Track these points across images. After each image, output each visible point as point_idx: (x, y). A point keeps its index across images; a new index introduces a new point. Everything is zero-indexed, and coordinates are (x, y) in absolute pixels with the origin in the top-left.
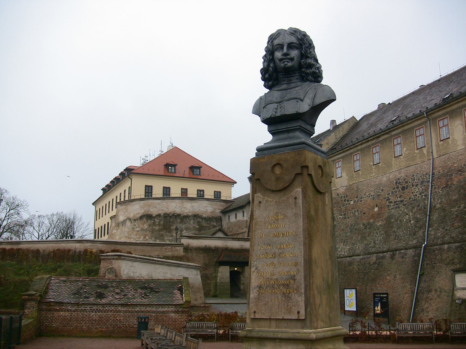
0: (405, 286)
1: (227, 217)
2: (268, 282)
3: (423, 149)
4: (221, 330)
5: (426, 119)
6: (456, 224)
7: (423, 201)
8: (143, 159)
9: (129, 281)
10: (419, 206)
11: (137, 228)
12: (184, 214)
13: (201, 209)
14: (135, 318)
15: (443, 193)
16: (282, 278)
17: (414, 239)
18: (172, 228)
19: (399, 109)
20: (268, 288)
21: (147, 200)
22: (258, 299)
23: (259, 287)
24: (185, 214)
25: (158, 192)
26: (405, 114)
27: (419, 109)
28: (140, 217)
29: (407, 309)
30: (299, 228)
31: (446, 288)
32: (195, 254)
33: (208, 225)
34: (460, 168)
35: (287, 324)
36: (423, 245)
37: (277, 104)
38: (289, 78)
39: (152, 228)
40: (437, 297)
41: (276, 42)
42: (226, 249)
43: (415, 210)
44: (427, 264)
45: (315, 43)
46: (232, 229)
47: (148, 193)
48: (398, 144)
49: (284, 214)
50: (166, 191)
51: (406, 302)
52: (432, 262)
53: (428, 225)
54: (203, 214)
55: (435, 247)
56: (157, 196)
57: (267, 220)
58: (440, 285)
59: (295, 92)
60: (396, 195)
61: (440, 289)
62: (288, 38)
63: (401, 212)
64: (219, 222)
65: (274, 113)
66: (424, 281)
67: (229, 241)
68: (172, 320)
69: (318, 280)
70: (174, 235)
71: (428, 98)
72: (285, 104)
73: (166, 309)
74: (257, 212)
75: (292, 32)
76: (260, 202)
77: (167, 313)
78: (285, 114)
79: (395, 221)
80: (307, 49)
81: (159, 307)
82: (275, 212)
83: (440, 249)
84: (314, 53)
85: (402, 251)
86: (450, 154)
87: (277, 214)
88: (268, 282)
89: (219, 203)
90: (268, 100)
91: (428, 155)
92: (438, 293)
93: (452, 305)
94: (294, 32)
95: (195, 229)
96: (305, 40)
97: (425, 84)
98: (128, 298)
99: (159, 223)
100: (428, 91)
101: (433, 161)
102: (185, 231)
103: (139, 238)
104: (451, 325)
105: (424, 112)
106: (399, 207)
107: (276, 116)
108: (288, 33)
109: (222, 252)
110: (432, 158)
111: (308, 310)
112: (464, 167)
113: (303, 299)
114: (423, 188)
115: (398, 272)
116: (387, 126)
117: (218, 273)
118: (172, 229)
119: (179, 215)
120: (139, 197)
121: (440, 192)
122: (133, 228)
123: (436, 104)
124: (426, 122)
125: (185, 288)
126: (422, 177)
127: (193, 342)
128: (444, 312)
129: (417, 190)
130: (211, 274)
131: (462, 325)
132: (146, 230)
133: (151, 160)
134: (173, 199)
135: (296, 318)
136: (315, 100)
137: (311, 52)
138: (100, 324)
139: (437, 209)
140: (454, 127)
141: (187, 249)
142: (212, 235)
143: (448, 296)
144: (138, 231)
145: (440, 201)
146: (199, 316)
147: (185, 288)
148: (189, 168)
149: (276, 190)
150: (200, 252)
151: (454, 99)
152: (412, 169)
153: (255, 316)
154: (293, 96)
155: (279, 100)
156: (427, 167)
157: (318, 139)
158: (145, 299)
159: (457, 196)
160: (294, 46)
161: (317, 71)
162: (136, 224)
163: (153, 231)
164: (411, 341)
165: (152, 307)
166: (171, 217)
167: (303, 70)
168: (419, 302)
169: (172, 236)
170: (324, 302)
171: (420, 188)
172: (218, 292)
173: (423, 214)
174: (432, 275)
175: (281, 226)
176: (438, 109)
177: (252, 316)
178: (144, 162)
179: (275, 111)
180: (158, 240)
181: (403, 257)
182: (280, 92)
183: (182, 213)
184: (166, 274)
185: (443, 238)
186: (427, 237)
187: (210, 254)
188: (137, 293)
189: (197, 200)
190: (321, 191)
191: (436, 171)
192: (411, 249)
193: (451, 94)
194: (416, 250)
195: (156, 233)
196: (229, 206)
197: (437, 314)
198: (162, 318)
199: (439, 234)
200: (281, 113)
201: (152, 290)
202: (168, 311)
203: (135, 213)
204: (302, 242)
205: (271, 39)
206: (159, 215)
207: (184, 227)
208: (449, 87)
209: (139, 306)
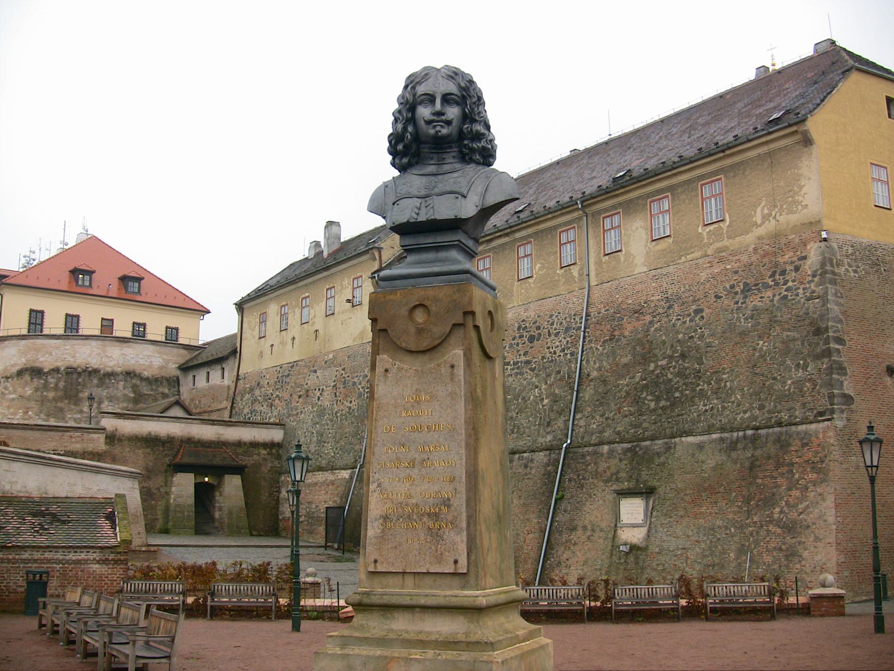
0: (528, 520)
1: (190, 377)
2: (400, 510)
3: (571, 267)
4: (190, 596)
5: (581, 212)
6: (625, 409)
7: (566, 363)
8: (25, 257)
9: (8, 499)
10: (559, 372)
11: (10, 393)
12: (107, 368)
13: (140, 361)
14: (21, 573)
15: (605, 351)
16: (426, 502)
17: (548, 433)
18: (81, 395)
19: (531, 191)
20: (401, 520)
21: (33, 339)
22: (382, 538)
23: (384, 519)
24: (109, 370)
25: (54, 323)
26: (541, 200)
27: (568, 193)
28: (18, 371)
29: (530, 561)
30: (459, 417)
31: (603, 525)
32: (128, 449)
33: (152, 393)
34: (638, 308)
35: (435, 580)
36: (565, 445)
37: (420, 200)
39: (42, 396)
40: (586, 539)
41: (421, 90)
42: (189, 441)
43: (552, 379)
44: (570, 480)
45: (486, 97)
46: (200, 402)
47: (36, 324)
48: (526, 256)
49: (431, 392)
50: (72, 322)
51: (530, 548)
52: (578, 477)
53: (575, 409)
54: (144, 370)
55: (586, 449)
56: (53, 332)
57: (399, 401)
58: (592, 519)
59: (452, 180)
60: (518, 351)
61: (593, 525)
62: (443, 85)
63: (525, 382)
64: (174, 387)
65: (415, 216)
66: (564, 511)
67: (196, 425)
68: (94, 577)
69: (486, 509)
70: (86, 409)
71: (586, 175)
72: (436, 201)
73: (83, 556)
74: (380, 388)
75: (450, 73)
76: (386, 371)
77: (84, 564)
79: (514, 399)
80: (474, 106)
81: (70, 552)
82: (414, 389)
83: (595, 453)
85: (525, 455)
86: (621, 280)
87: (418, 393)
88: (400, 510)
89: (175, 350)
90: (401, 190)
91: (581, 280)
92: (589, 533)
93: (612, 555)
94: (453, 75)
95: (126, 398)
96: (471, 89)
97: (581, 147)
98: (7, 534)
99: (56, 385)
100: (585, 161)
101: (589, 290)
102: (106, 403)
103: (15, 414)
104: (616, 590)
105: (578, 199)
106: (521, 374)
108: (444, 75)
109: (181, 446)
110: (587, 287)
111: (473, 558)
112: (645, 305)
113: (465, 539)
114: (569, 339)
115: (515, 493)
116: (507, 221)
117: (171, 486)
118: (83, 398)
119: (96, 371)
120: (18, 333)
121: (598, 349)
122: (3, 393)
123: (601, 186)
124: (579, 219)
125: (121, 515)
126: (568, 320)
127: (165, 619)
128: (598, 567)
129: (557, 343)
130: (158, 489)
131: (635, 590)
132: (29, 399)
133: (42, 260)
134: (87, 339)
135: (452, 571)
136: (487, 197)
137: (480, 113)
138: (97, 580)
139: (591, 380)
140: (630, 232)
141: (112, 438)
142: (162, 413)
143: (606, 539)
144: (13, 399)
145: (597, 365)
146: (141, 570)
147: (121, 515)
148: (119, 279)
149: (418, 350)
150: (139, 444)
151: (635, 180)
152: (549, 304)
153: (375, 567)
154: (448, 189)
155: (423, 193)
156: (577, 303)
157: (374, 237)
158: (41, 535)
159: (630, 357)
160: (453, 99)
161: (490, 147)
162: (9, 385)
163: (43, 401)
164: (544, 618)
165: (56, 552)
166: (79, 374)
167: (466, 142)
168: (552, 549)
169: (81, 412)
170: (494, 545)
171: (563, 340)
172: (170, 524)
173: (566, 388)
174: (579, 500)
175: (424, 413)
176: (604, 197)
177: (371, 569)
178: (28, 263)
180: (52, 419)
181: (526, 466)
182: (424, 179)
183: (101, 366)
184: (75, 487)
185: (601, 432)
186: (573, 430)
187: (158, 450)
188: (24, 523)
189: (133, 342)
190: (491, 355)
191: (593, 311)
192: (541, 451)
193: (629, 171)
194: (550, 454)
195: (49, 404)
196: (196, 356)
197: (586, 570)
198: (74, 572)
199: (595, 426)
200: (427, 216)
201: (55, 518)
202: (87, 560)
203: (8, 364)
204: (463, 443)
205: (411, 83)
206: (57, 370)
207: (105, 394)
208: (626, 158)
209: (28, 549)
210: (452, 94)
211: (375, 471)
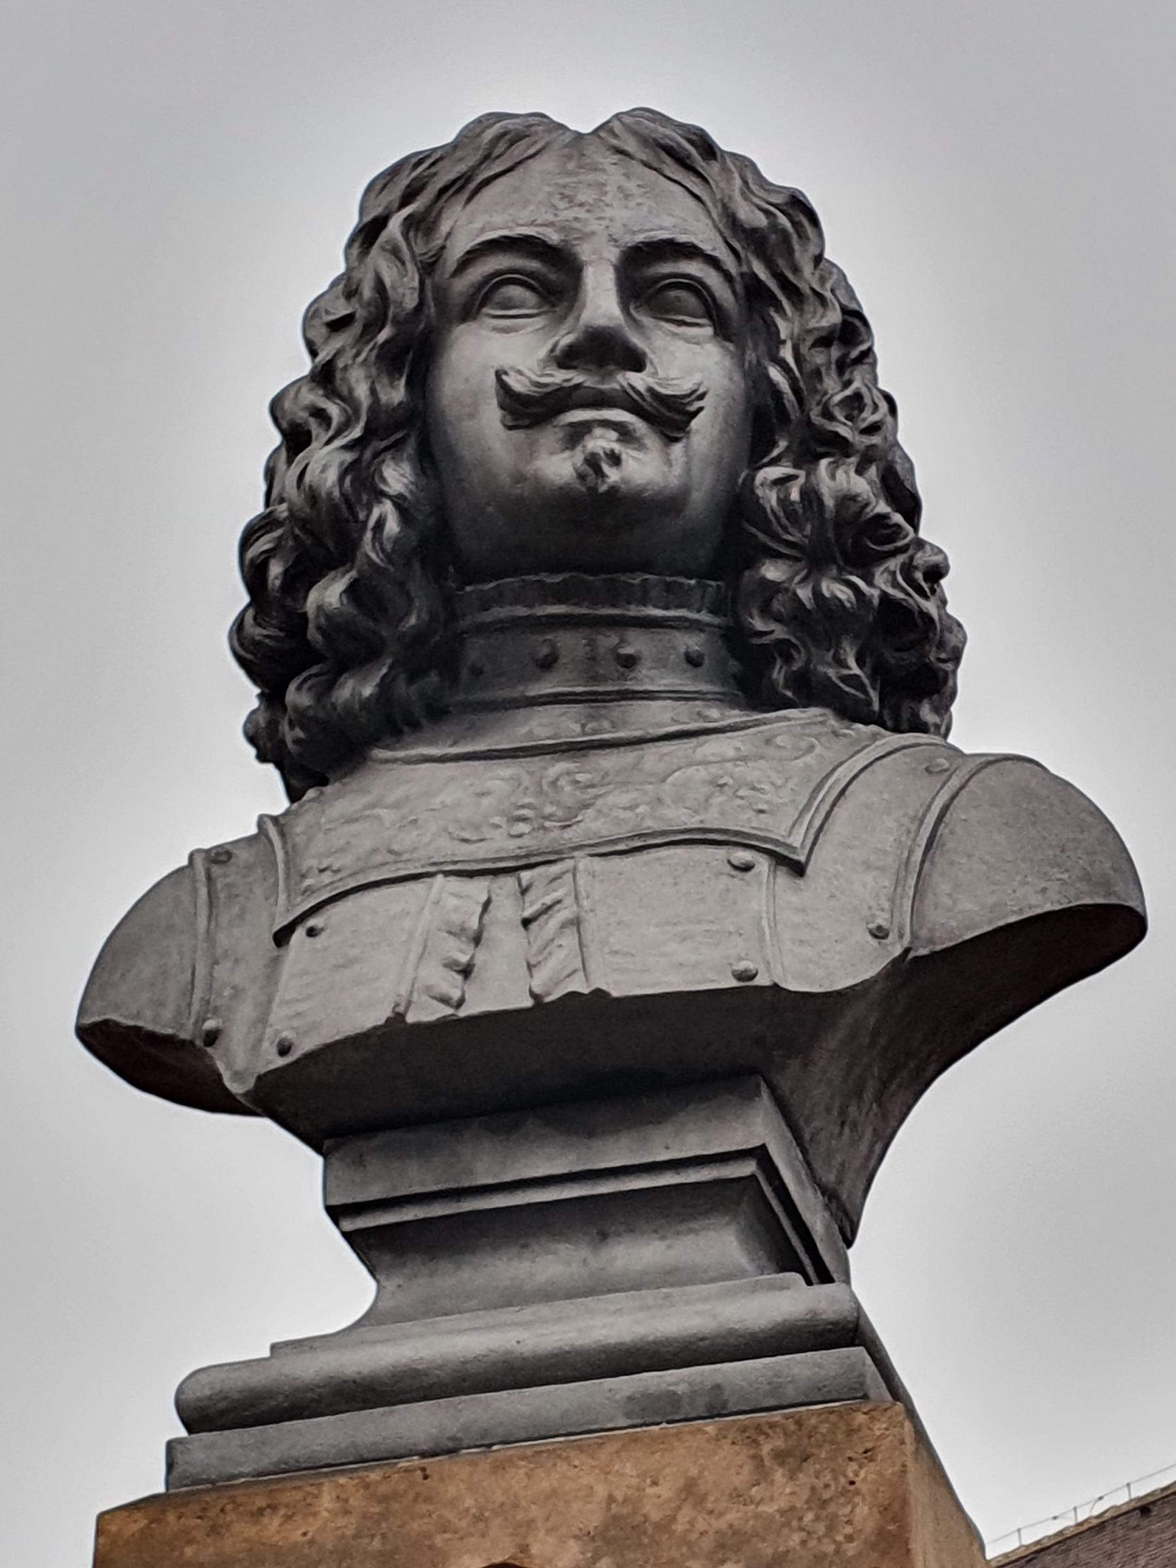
37: (478, 889)
38: (607, 640)
65: (452, 985)
78: (599, 993)
84: (889, 419)
107: (463, 1013)
136: (941, 886)
154: (681, 817)
160: (696, 287)
167: (773, 572)
179: (464, 959)
210: (690, 251)
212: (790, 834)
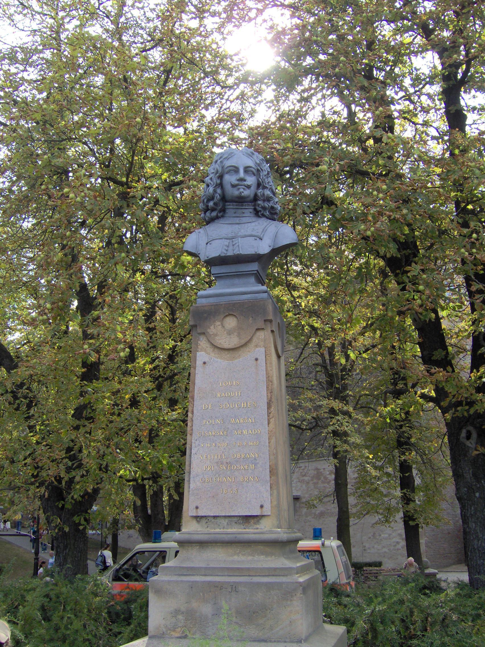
37: (228, 241)
65: (225, 252)
153: (197, 512)
210: (251, 167)
211: (196, 438)
212: (198, 518)
